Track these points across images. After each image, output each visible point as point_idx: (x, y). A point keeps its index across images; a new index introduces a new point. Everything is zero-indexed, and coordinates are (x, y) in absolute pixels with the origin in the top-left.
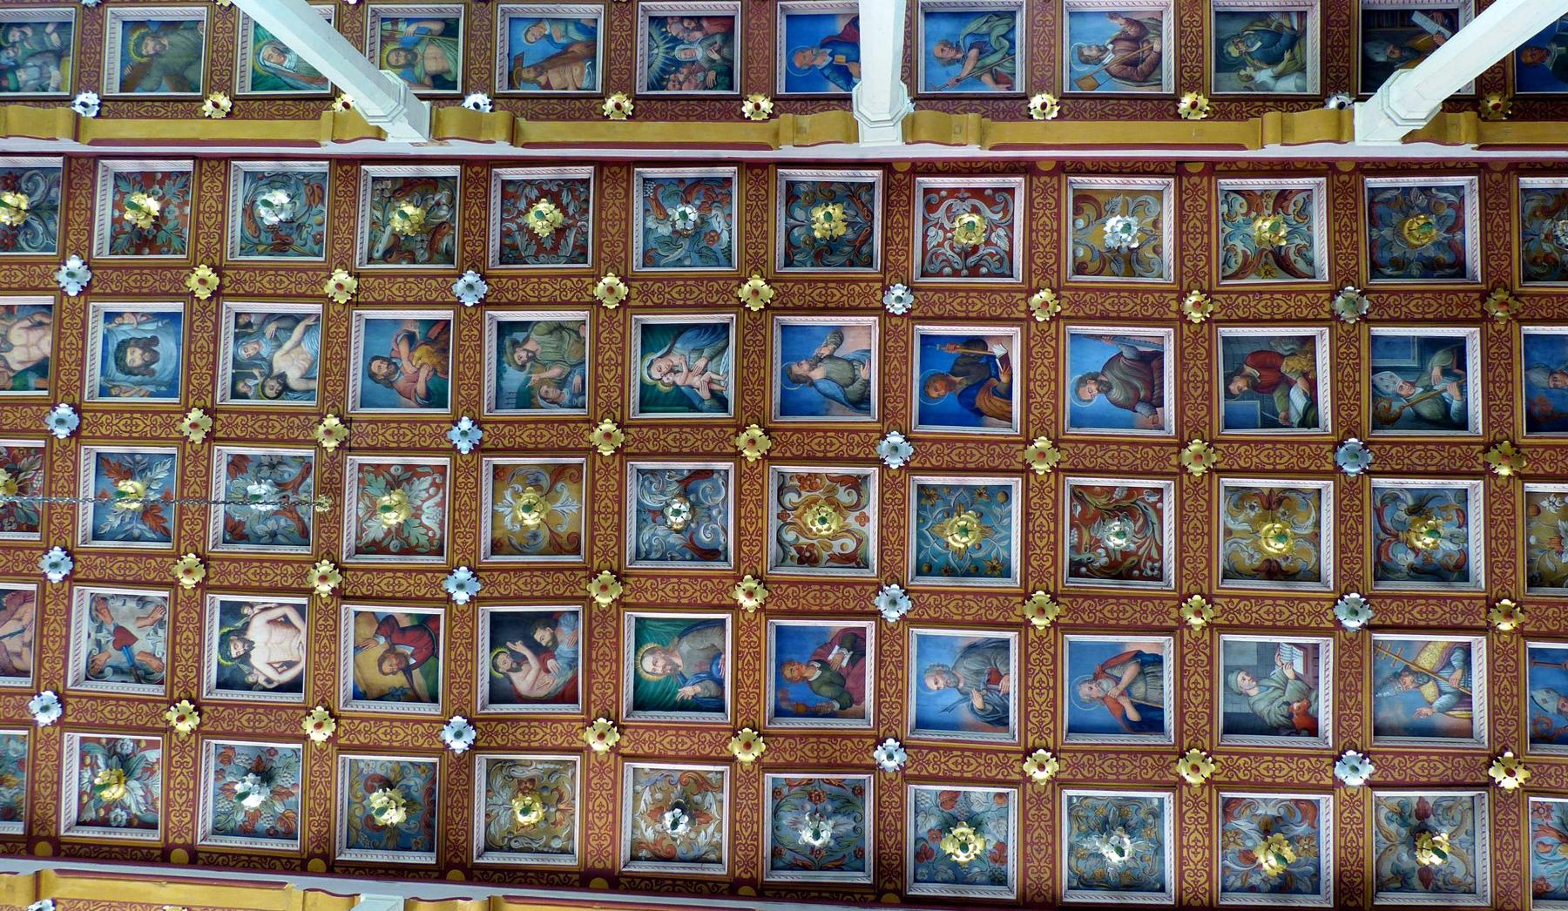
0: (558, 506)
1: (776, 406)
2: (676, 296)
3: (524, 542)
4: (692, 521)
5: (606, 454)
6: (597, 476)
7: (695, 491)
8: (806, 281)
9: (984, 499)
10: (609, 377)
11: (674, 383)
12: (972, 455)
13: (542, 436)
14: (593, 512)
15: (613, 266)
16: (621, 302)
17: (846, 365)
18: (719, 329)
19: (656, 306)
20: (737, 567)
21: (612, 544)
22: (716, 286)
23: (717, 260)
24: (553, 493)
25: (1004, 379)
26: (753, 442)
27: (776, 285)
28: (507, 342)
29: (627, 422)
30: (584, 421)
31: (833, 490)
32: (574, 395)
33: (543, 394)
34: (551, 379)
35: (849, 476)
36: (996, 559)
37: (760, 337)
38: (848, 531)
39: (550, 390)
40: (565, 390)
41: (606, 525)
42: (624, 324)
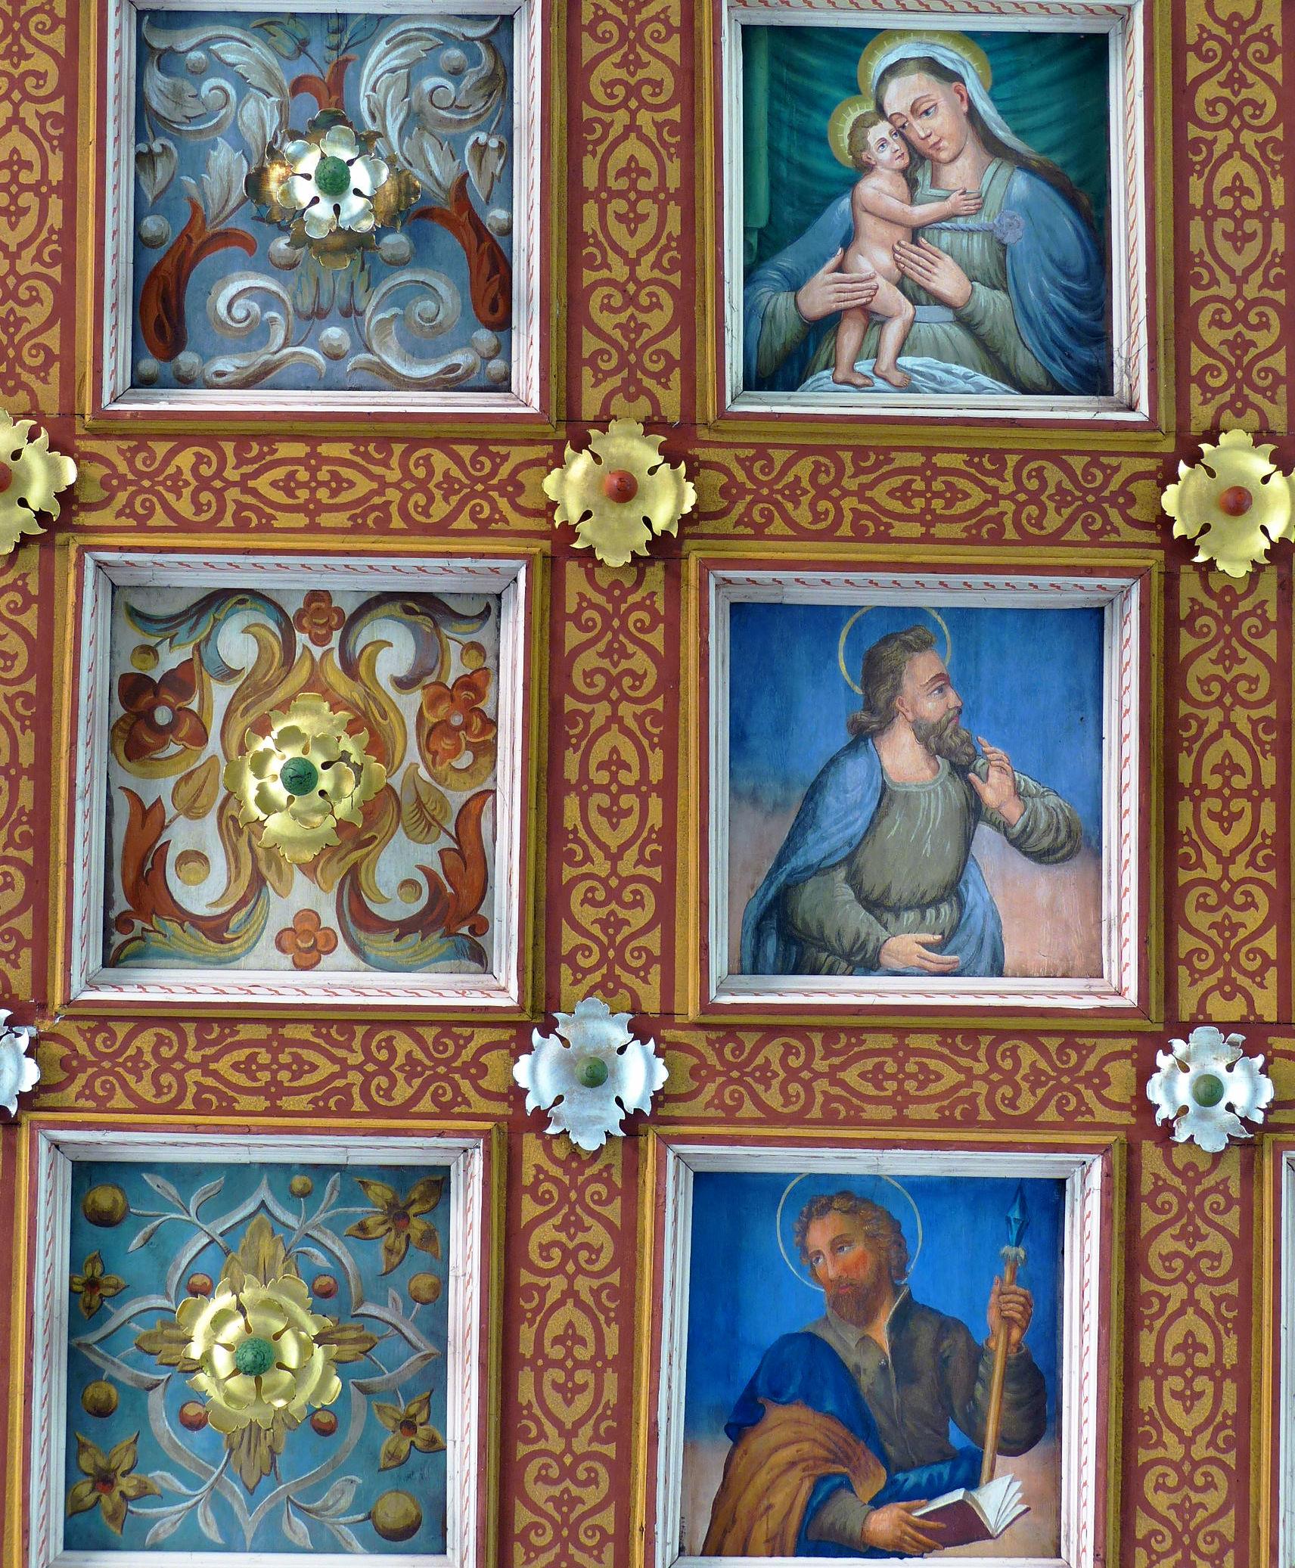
4: (301, 241)
7: (420, 254)
9: (390, 1441)
11: (865, 168)
12: (569, 1392)
17: (937, 875)
18: (1085, 355)
19: (1183, 92)
20: (108, 427)
25: (884, 1522)
31: (426, 822)
36: (144, 1492)
38: (258, 881)
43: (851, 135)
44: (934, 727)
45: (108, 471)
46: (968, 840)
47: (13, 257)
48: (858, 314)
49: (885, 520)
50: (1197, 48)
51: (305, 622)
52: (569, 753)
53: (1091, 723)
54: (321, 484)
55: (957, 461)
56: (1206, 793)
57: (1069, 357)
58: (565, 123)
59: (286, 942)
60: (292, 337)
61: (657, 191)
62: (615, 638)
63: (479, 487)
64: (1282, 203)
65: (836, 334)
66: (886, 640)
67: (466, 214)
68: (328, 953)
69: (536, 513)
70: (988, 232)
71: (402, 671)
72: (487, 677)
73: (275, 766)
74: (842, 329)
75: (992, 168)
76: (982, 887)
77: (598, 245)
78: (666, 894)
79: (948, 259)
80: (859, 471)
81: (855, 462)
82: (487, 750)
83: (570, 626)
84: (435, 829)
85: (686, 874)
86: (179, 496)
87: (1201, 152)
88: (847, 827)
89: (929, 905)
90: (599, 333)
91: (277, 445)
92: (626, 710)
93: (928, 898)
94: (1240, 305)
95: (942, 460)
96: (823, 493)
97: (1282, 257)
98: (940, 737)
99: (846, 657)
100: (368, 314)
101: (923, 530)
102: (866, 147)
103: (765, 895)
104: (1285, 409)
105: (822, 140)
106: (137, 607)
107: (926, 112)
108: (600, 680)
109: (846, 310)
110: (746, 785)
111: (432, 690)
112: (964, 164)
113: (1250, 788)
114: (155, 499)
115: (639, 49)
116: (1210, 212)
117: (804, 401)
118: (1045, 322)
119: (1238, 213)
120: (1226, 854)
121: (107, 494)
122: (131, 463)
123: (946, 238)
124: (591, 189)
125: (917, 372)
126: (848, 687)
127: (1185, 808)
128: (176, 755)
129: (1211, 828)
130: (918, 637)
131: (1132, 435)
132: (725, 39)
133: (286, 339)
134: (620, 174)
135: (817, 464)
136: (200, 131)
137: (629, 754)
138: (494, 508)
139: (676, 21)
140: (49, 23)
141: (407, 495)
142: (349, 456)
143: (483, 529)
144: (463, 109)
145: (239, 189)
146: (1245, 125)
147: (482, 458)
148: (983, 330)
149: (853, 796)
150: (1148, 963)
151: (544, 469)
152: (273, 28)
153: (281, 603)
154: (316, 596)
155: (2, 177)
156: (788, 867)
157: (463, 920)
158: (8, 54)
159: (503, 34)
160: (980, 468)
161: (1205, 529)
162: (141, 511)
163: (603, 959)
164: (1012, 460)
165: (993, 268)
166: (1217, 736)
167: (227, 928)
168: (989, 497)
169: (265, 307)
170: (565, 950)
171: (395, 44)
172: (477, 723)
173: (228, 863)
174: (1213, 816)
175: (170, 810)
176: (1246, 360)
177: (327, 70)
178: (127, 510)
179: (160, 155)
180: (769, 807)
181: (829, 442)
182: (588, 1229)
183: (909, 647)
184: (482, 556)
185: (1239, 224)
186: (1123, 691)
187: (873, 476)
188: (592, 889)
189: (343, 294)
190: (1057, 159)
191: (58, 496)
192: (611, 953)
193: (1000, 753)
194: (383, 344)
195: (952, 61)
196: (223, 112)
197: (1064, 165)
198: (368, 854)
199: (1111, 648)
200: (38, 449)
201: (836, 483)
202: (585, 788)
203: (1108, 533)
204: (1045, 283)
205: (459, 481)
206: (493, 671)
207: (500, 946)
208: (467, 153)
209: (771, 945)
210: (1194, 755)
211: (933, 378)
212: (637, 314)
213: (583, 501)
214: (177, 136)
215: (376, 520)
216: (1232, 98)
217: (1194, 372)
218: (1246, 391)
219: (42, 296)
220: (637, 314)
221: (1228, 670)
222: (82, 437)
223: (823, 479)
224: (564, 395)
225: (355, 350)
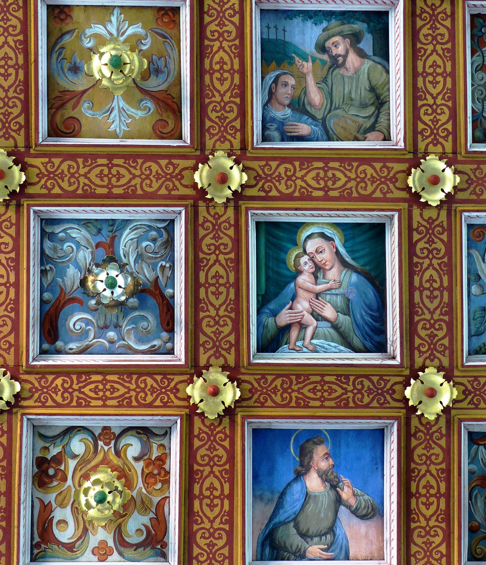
0: (119, 102)
1: (264, 424)
2: (426, 276)
3: (67, 53)
4: (99, 303)
5: (197, 177)
6: (163, 162)
7: (142, 306)
8: (449, 465)
10: (308, 178)
11: (299, 272)
13: (222, 80)
14: (110, 157)
15: (469, 182)
16: (417, 196)
17: (325, 525)
18: (377, 338)
19: (412, 246)
20: (32, 370)
21: (65, 185)
22: (441, 334)
23: (479, 334)
24: (138, 95)
26: (216, 392)
27: (442, 422)
28: (359, 26)
29: (244, 205)
30: (243, 142)
31: (144, 507)
32: (281, 125)
33: (283, 79)
34: (305, 91)
35: (166, 532)
37: (366, 400)
38: (85, 530)
39: (289, 90)
40: (288, 111)
41: (92, 176)
42: (385, 200)
43: (294, 261)
44: (324, 472)
45: (31, 386)
46: (336, 512)
47: (6, 91)
48: (297, 324)
49: (307, 400)
50: (417, 230)
51: (102, 438)
52: (196, 485)
53: (380, 469)
54: (107, 390)
55: (332, 379)
56: (421, 495)
57: (372, 339)
58: (193, 259)
59: (95, 552)
60: (96, 336)
61: (226, 283)
62: (212, 444)
63: (163, 390)
64: (447, 284)
65: (289, 332)
66: (307, 441)
67: (158, 291)
68: (110, 555)
69: (184, 399)
70: (343, 295)
71: (136, 454)
72: (166, 456)
73: (92, 493)
74: (291, 330)
75: (345, 271)
76: (342, 529)
77: (205, 303)
78: (230, 534)
79: (329, 304)
80: (298, 383)
81: (296, 380)
82: (166, 482)
83: (196, 439)
84: (148, 511)
85: (237, 527)
86: (57, 395)
87: (418, 267)
88: (294, 507)
89: (323, 535)
90: (205, 334)
91: (92, 376)
92: (216, 469)
93: (322, 533)
94: (432, 322)
95: (327, 379)
96: (285, 391)
97: (447, 304)
98: (327, 475)
99: (293, 447)
100: (123, 327)
101: (321, 403)
102: (300, 265)
103: (265, 532)
104: (448, 359)
105: (284, 262)
106: (42, 433)
107: (321, 252)
108: (206, 459)
109: (293, 323)
110: (258, 493)
111: (147, 461)
112: (334, 270)
113: (436, 493)
114: (48, 396)
115: (219, 233)
116: (421, 289)
117: (279, 357)
118: (363, 327)
119: (431, 289)
120: (428, 517)
121: (31, 394)
122: (39, 383)
123: (328, 297)
124: (203, 283)
125: (318, 345)
126: (294, 458)
127: (413, 501)
128: (57, 485)
129: (423, 508)
130: (319, 440)
131: (394, 369)
132: (250, 228)
133: (94, 336)
134: (213, 278)
135: (283, 381)
136: (63, 262)
137: (217, 484)
138: (169, 398)
139: (232, 222)
140: (9, 225)
141: (138, 393)
142: (117, 380)
143: (165, 405)
144: (156, 253)
145: (77, 283)
146: (434, 257)
147: (164, 380)
148: (342, 330)
149: (296, 496)
150: (400, 557)
151: (186, 384)
152: (89, 225)
153: (93, 431)
154: (106, 428)
155: (3, 63)
156: (273, 522)
157: (158, 543)
158: (2, 19)
159: (171, 226)
160: (341, 381)
161: (420, 403)
162: (43, 400)
163: (208, 558)
164: (352, 378)
165: (345, 307)
166: (424, 475)
167: (74, 547)
168: (344, 391)
169: (87, 325)
170: (195, 555)
171: (133, 230)
172: (163, 473)
173: (75, 524)
174: (423, 503)
175: (54, 505)
176: (434, 341)
177: (108, 239)
178: (38, 400)
179: (49, 270)
180: (266, 501)
181: (287, 373)
182: (216, 117)
183: (316, 444)
184: (165, 415)
185: (432, 292)
186: (391, 459)
187: (303, 385)
188: (204, 533)
189: (114, 320)
190: (367, 268)
191: (14, 396)
192: (211, 556)
193: (348, 480)
194: (129, 338)
195: (330, 233)
196: (71, 255)
197: (370, 270)
198: (124, 520)
199: (387, 443)
200: (7, 379)
201: (290, 387)
202: (201, 497)
203: (386, 403)
204: (363, 312)
205: (156, 388)
206: (168, 454)
207: (171, 552)
208: (158, 269)
209: (267, 551)
210: (416, 482)
211: (324, 347)
212: (219, 328)
213: (200, 396)
214: (55, 264)
215: (127, 403)
216: (429, 247)
217: (416, 346)
218: (435, 352)
219: (8, 323)
220: (219, 328)
221: (428, 452)
222: (22, 374)
223: (285, 386)
224: (193, 357)
225: (119, 340)
